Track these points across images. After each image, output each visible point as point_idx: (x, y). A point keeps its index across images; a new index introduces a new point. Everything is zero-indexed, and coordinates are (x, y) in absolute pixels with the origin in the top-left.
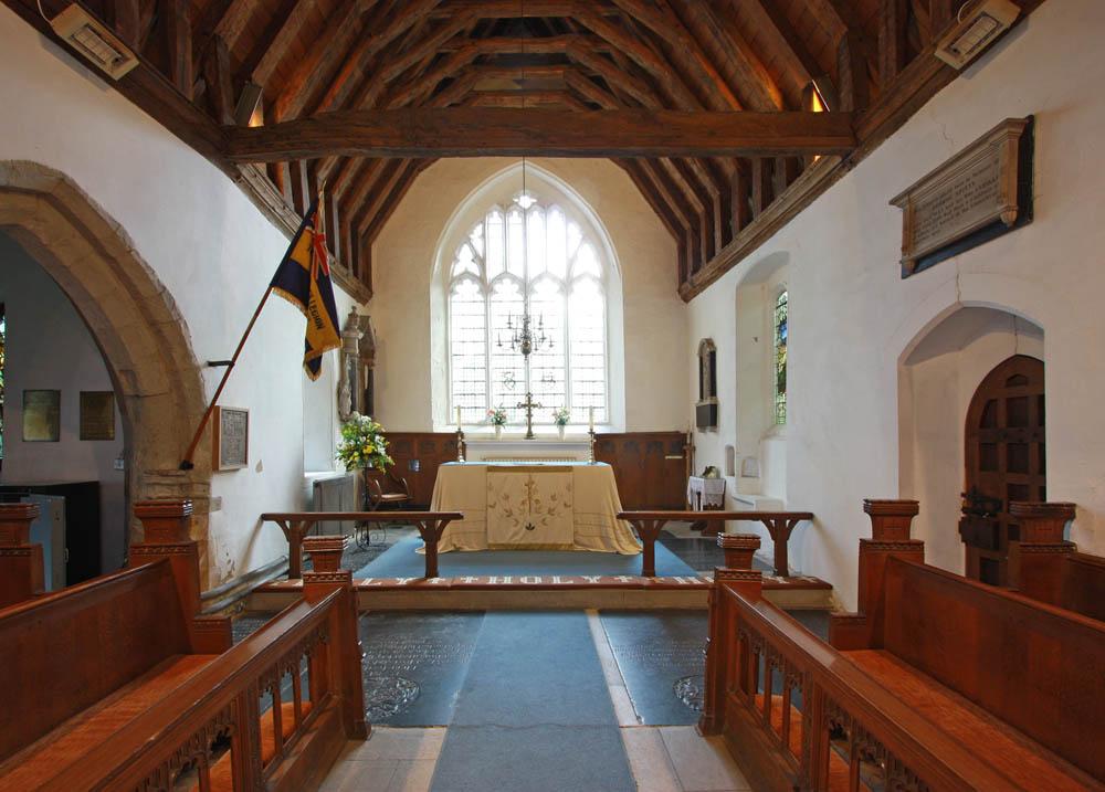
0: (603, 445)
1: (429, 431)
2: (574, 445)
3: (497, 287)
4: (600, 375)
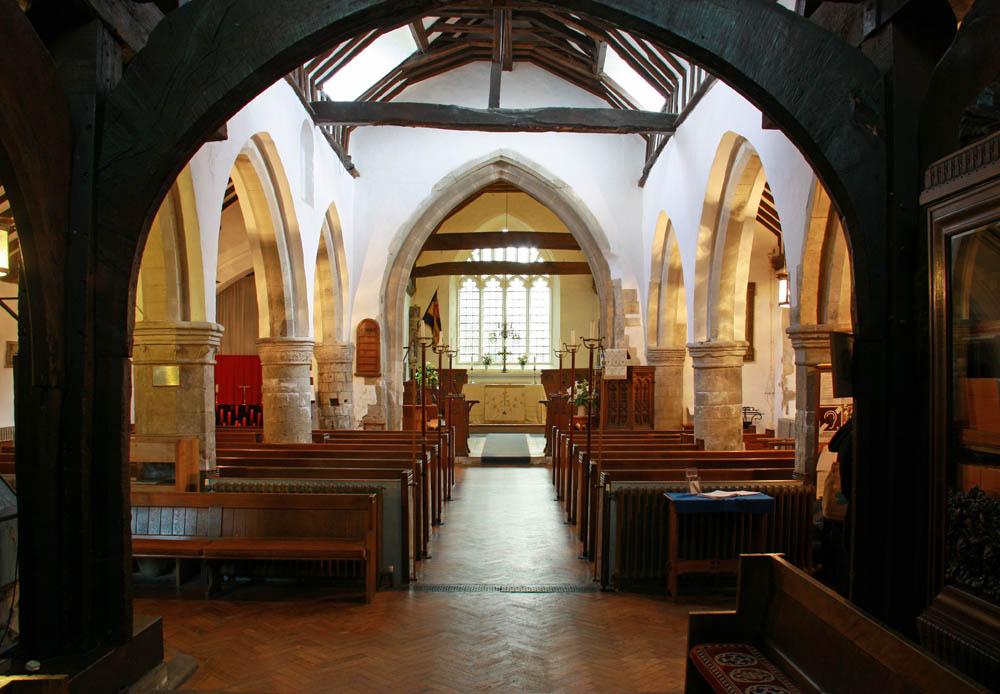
0: (546, 375)
2: (527, 376)
4: (547, 335)
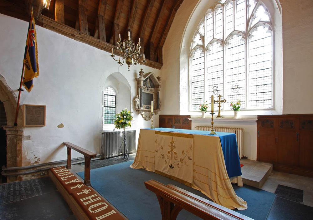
1: (179, 115)
3: (210, 48)
